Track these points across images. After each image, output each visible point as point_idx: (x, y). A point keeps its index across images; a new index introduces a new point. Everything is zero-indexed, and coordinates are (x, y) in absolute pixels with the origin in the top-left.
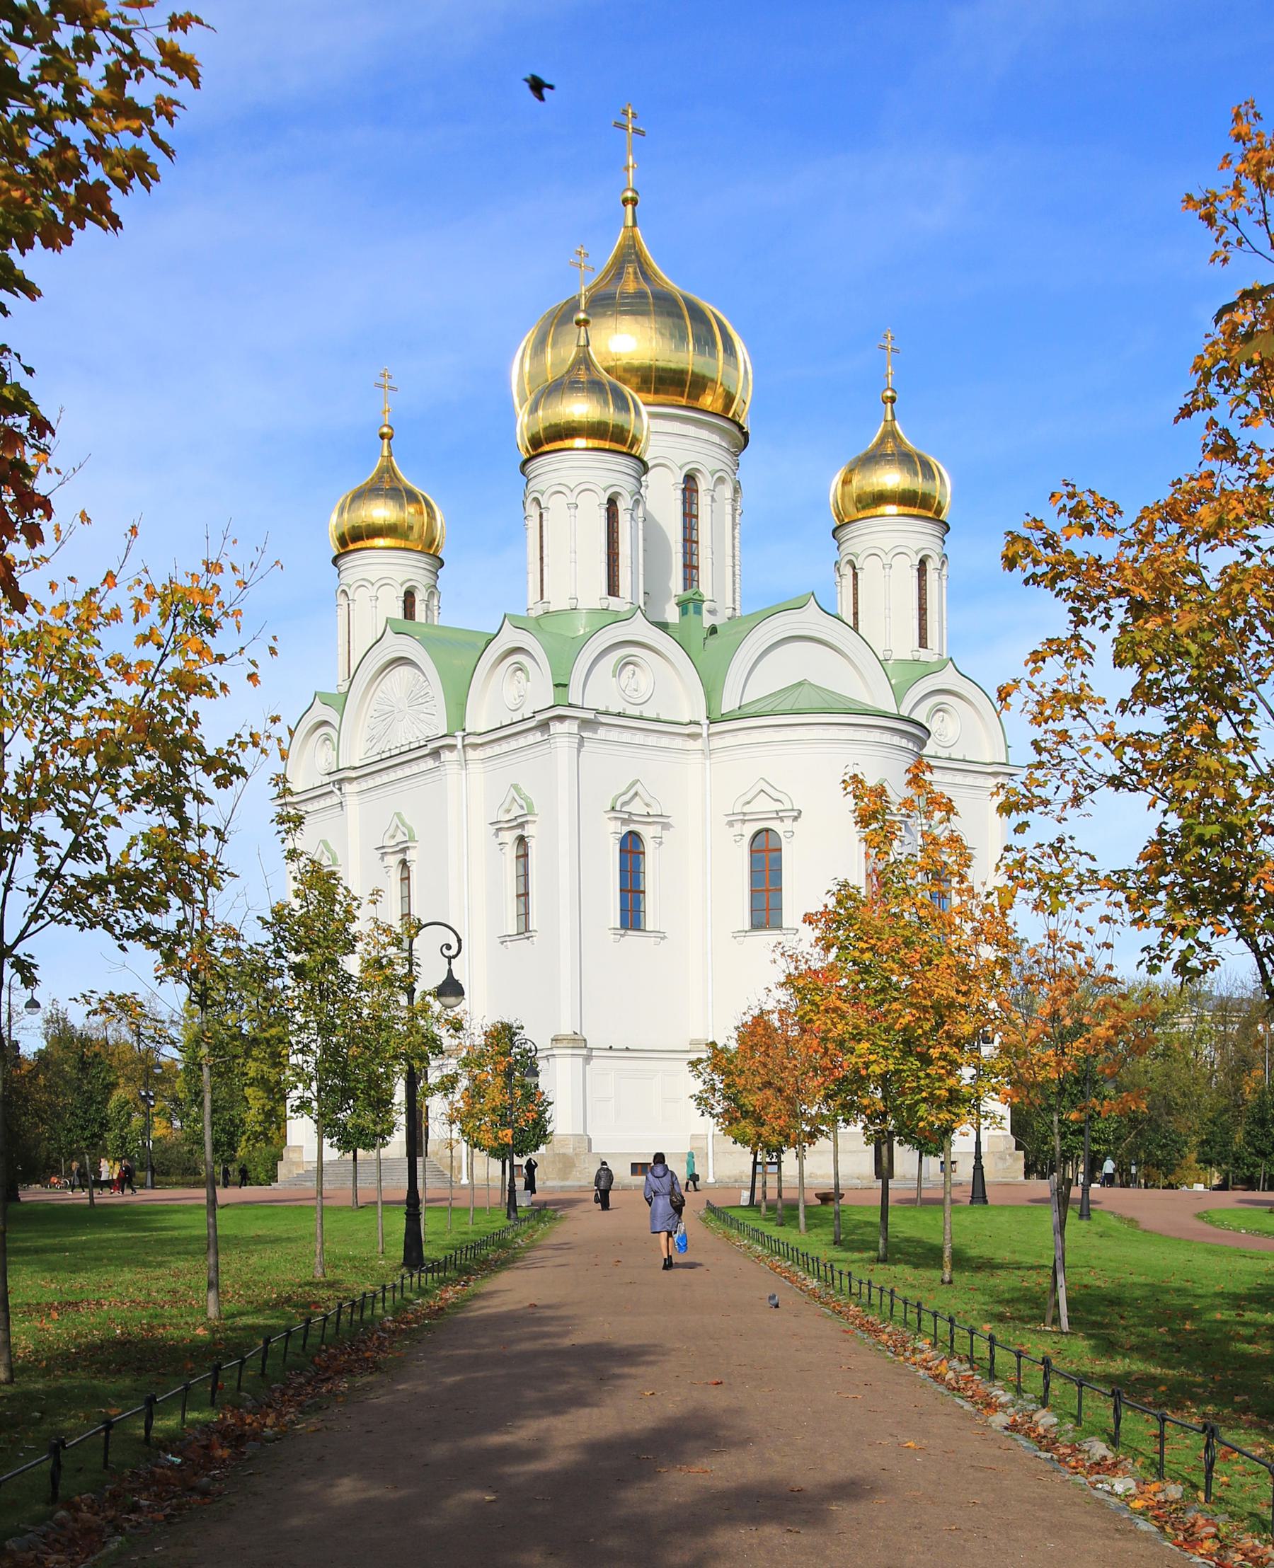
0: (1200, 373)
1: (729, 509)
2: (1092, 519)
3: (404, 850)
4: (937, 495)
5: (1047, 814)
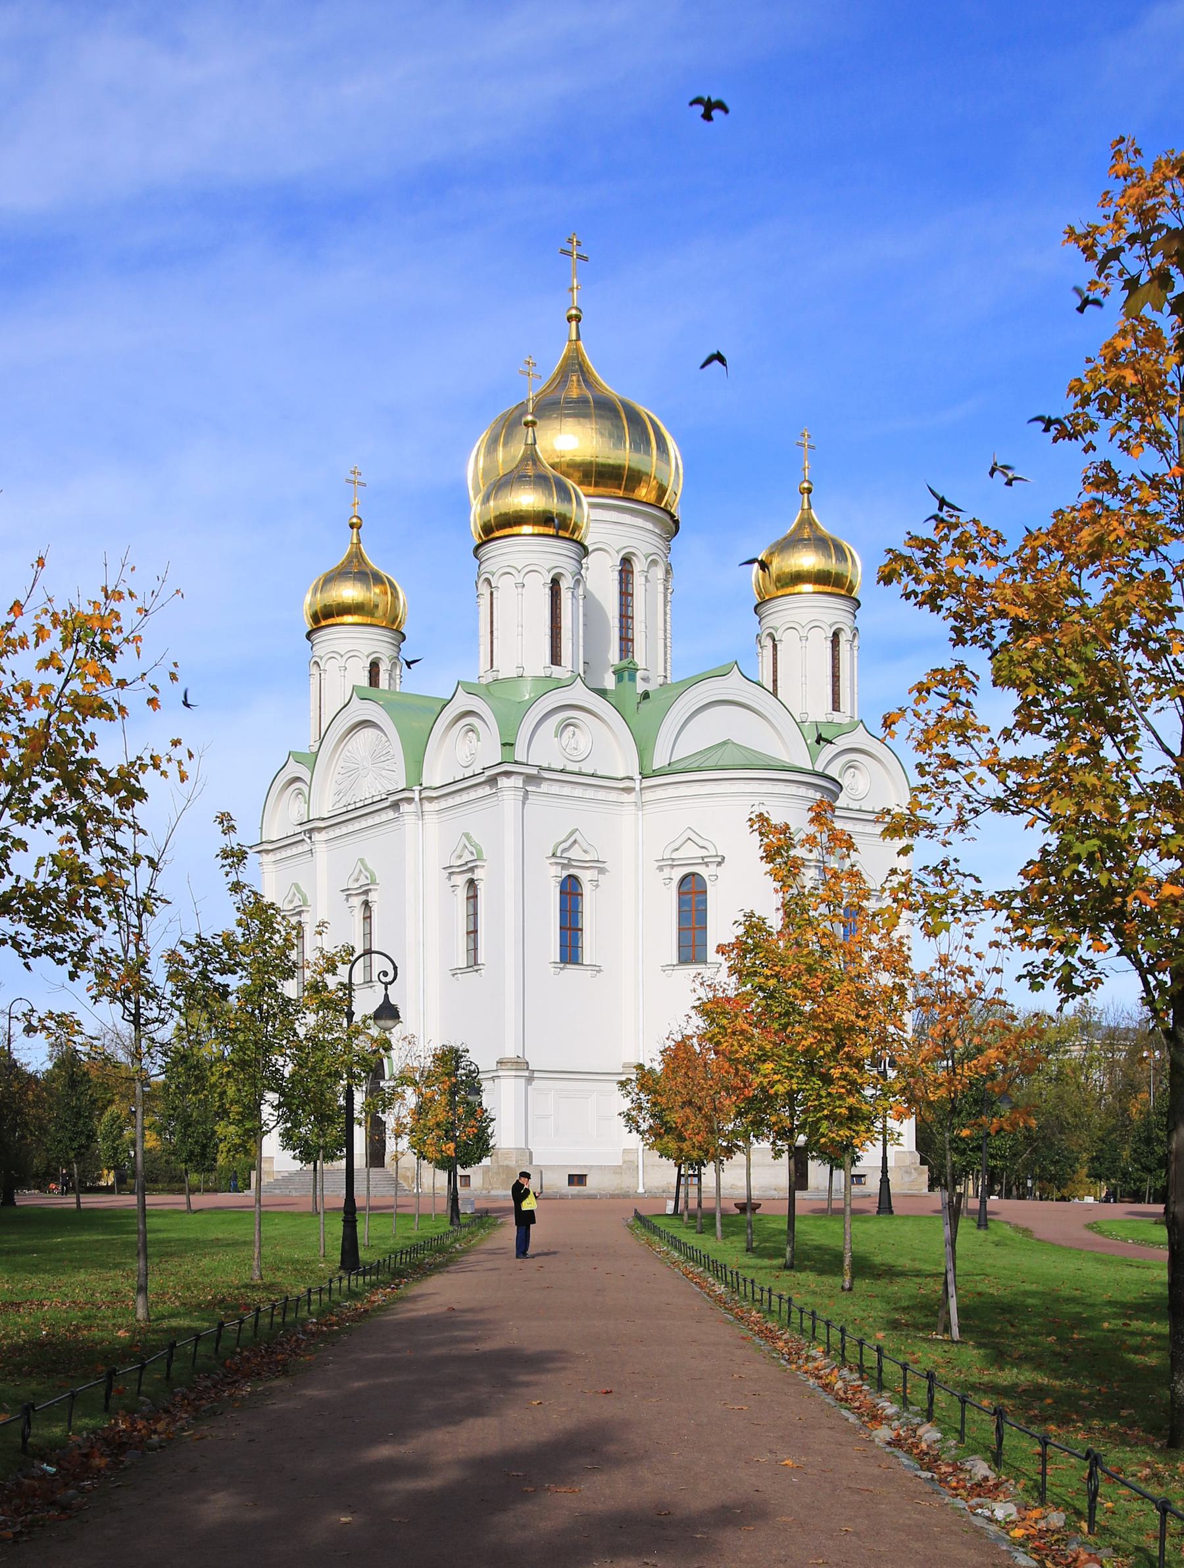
0: (1079, 396)
1: (661, 588)
2: (976, 549)
3: (366, 892)
4: (849, 574)
5: (932, 837)
